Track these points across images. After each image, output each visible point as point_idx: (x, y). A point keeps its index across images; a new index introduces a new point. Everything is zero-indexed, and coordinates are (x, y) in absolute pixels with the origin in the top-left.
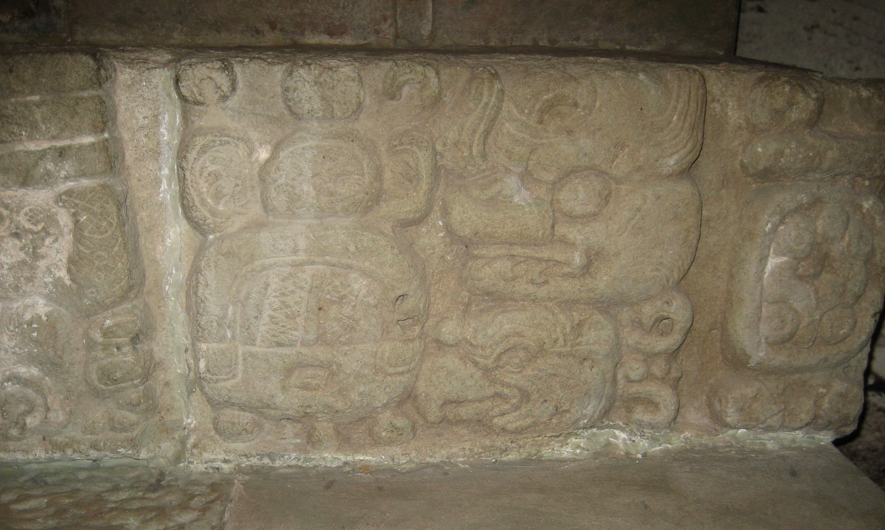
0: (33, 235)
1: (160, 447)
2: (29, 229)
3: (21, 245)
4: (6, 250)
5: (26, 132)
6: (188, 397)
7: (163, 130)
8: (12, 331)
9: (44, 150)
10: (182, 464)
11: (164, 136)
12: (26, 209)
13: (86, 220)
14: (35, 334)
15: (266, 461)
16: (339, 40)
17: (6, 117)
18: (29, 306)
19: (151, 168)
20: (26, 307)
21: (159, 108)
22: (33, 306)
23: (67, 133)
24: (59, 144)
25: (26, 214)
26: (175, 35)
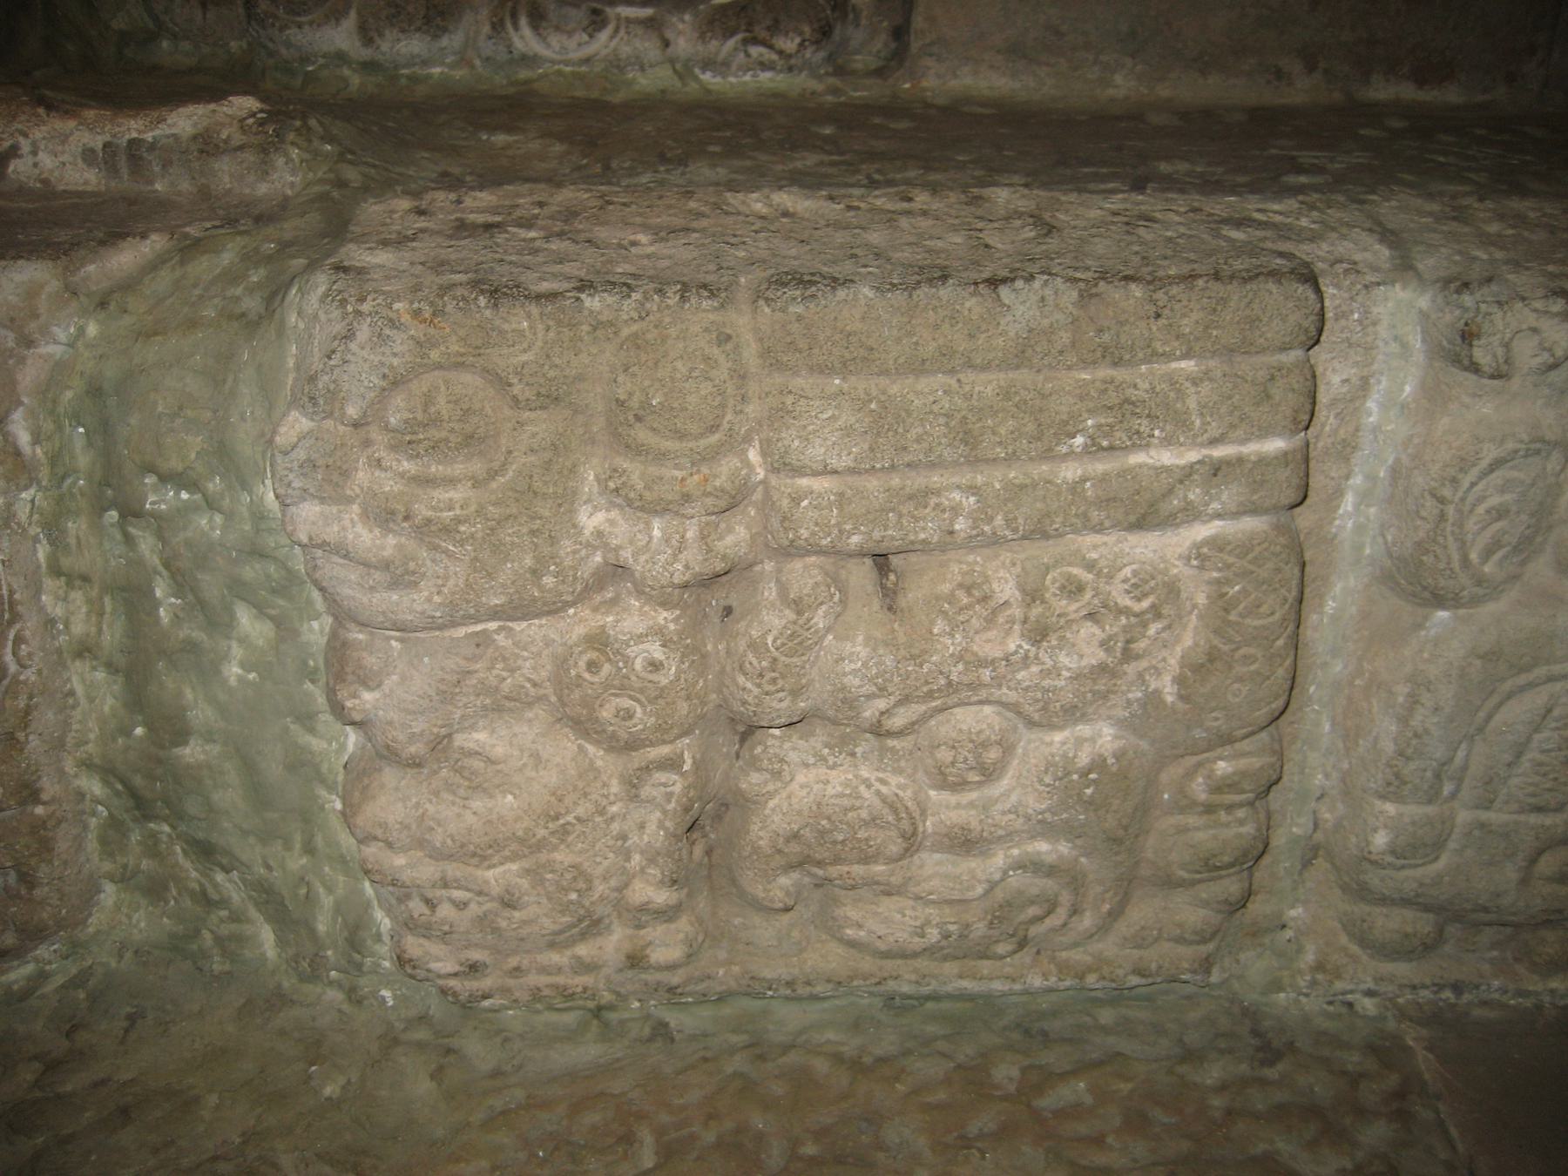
0: (1127, 618)
1: (1238, 961)
2: (1126, 607)
3: (1103, 636)
4: (1074, 645)
5: (1162, 430)
6: (1300, 873)
7: (1371, 404)
8: (1048, 785)
9: (1192, 465)
10: (1282, 995)
11: (1370, 415)
12: (1127, 571)
13: (1239, 592)
14: (1089, 791)
15: (1447, 994)
16: (1435, 93)
17: (1133, 403)
18: (1086, 740)
19: (1333, 474)
20: (1080, 742)
21: (1372, 364)
22: (1093, 740)
23: (1239, 433)
24: (1219, 452)
25: (1125, 581)
26: (1118, 79)
